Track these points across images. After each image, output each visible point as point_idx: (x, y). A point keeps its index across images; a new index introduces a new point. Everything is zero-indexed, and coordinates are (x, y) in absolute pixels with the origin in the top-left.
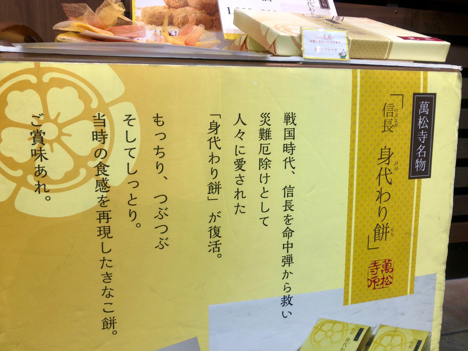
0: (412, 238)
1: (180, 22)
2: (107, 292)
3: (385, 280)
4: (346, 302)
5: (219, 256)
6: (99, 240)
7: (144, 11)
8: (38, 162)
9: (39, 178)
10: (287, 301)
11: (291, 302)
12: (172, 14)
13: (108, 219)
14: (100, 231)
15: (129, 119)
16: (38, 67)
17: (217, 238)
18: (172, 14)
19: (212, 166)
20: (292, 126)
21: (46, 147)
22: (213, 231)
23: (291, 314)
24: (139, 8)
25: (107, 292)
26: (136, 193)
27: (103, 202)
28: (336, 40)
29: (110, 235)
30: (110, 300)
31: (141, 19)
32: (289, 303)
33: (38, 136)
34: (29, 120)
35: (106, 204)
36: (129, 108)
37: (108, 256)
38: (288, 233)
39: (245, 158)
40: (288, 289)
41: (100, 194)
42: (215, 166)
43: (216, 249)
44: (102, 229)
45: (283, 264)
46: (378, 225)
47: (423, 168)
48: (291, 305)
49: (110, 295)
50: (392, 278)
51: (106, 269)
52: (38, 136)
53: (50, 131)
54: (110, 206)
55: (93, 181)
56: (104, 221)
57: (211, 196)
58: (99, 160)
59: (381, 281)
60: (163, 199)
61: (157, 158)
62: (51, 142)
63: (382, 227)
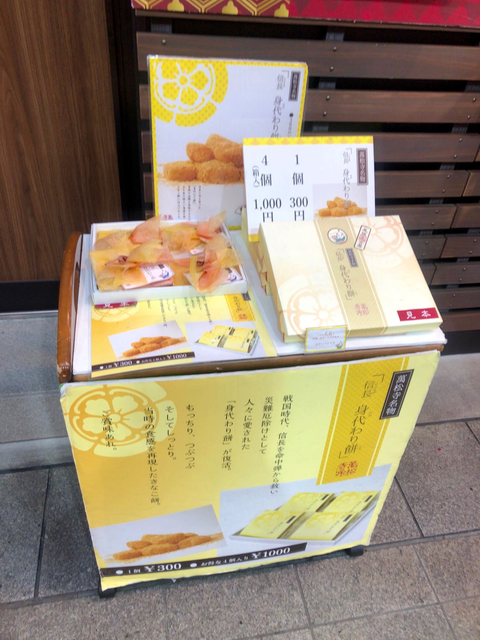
0: (376, 449)
1: (205, 176)
2: (154, 488)
4: (318, 483)
6: (149, 466)
7: (167, 167)
8: (108, 433)
9: (109, 440)
10: (210, 321)
12: (196, 169)
15: (169, 409)
16: (105, 386)
17: (228, 462)
18: (196, 169)
20: (290, 402)
21: (113, 426)
24: (161, 165)
25: (154, 488)
27: (151, 449)
28: (336, 335)
30: (156, 491)
31: (163, 175)
33: (107, 420)
34: (101, 414)
36: (171, 403)
38: (280, 455)
52: (107, 420)
53: (114, 418)
55: (145, 440)
57: (225, 442)
58: (148, 431)
62: (116, 424)
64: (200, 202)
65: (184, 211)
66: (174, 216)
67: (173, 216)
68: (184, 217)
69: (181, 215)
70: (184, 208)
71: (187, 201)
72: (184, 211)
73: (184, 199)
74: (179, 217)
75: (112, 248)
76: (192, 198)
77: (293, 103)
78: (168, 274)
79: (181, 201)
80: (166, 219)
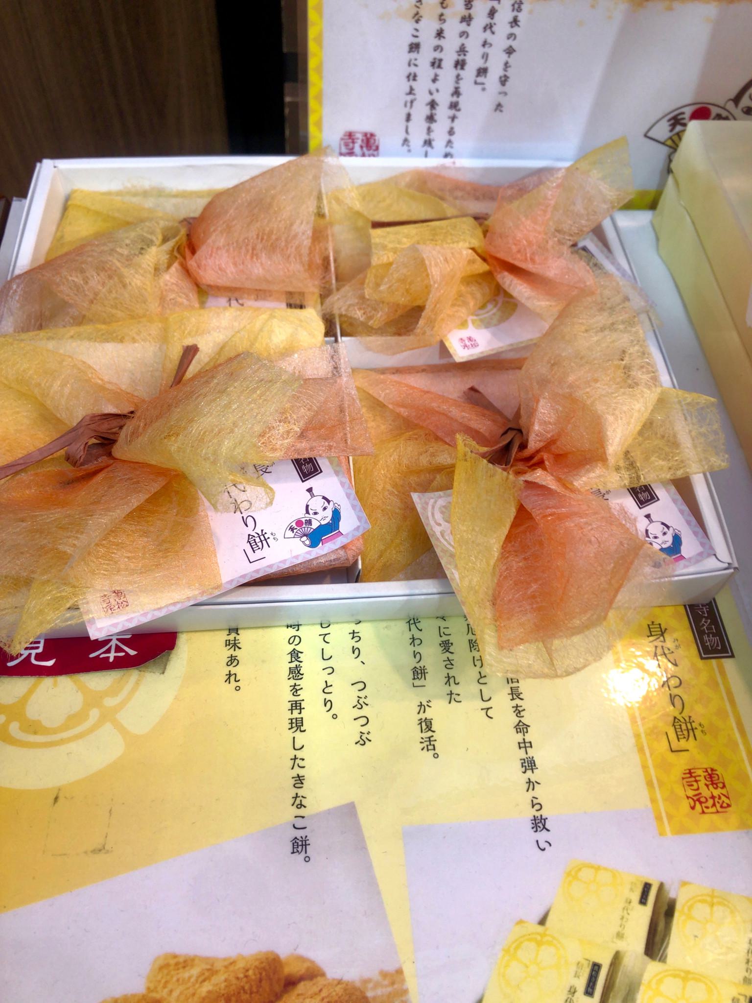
2: (298, 802)
3: (716, 800)
5: (436, 756)
6: (290, 734)
10: (539, 824)
11: (547, 826)
13: (301, 709)
14: (292, 723)
17: (430, 734)
19: (414, 649)
22: (424, 724)
23: (550, 845)
25: (298, 802)
26: (331, 679)
29: (302, 729)
30: (302, 812)
32: (544, 827)
35: (299, 692)
37: (299, 754)
39: (452, 639)
40: (537, 807)
41: (292, 682)
42: (417, 649)
43: (431, 747)
44: (294, 721)
45: (524, 769)
46: (675, 718)
47: (718, 645)
48: (548, 830)
49: (301, 805)
50: (728, 798)
51: (297, 771)
54: (303, 694)
56: (296, 712)
57: (417, 682)
59: (710, 802)
60: (361, 686)
61: (353, 643)
63: (682, 720)
64: (504, 80)
65: (431, 118)
66: (388, 139)
67: (383, 141)
68: (428, 143)
69: (418, 136)
70: (433, 104)
71: (448, 73)
72: (431, 118)
73: (436, 64)
74: (406, 141)
75: (80, 320)
76: (474, 61)
77: (641, 907)
78: (336, 515)
79: (425, 71)
80: (351, 153)
